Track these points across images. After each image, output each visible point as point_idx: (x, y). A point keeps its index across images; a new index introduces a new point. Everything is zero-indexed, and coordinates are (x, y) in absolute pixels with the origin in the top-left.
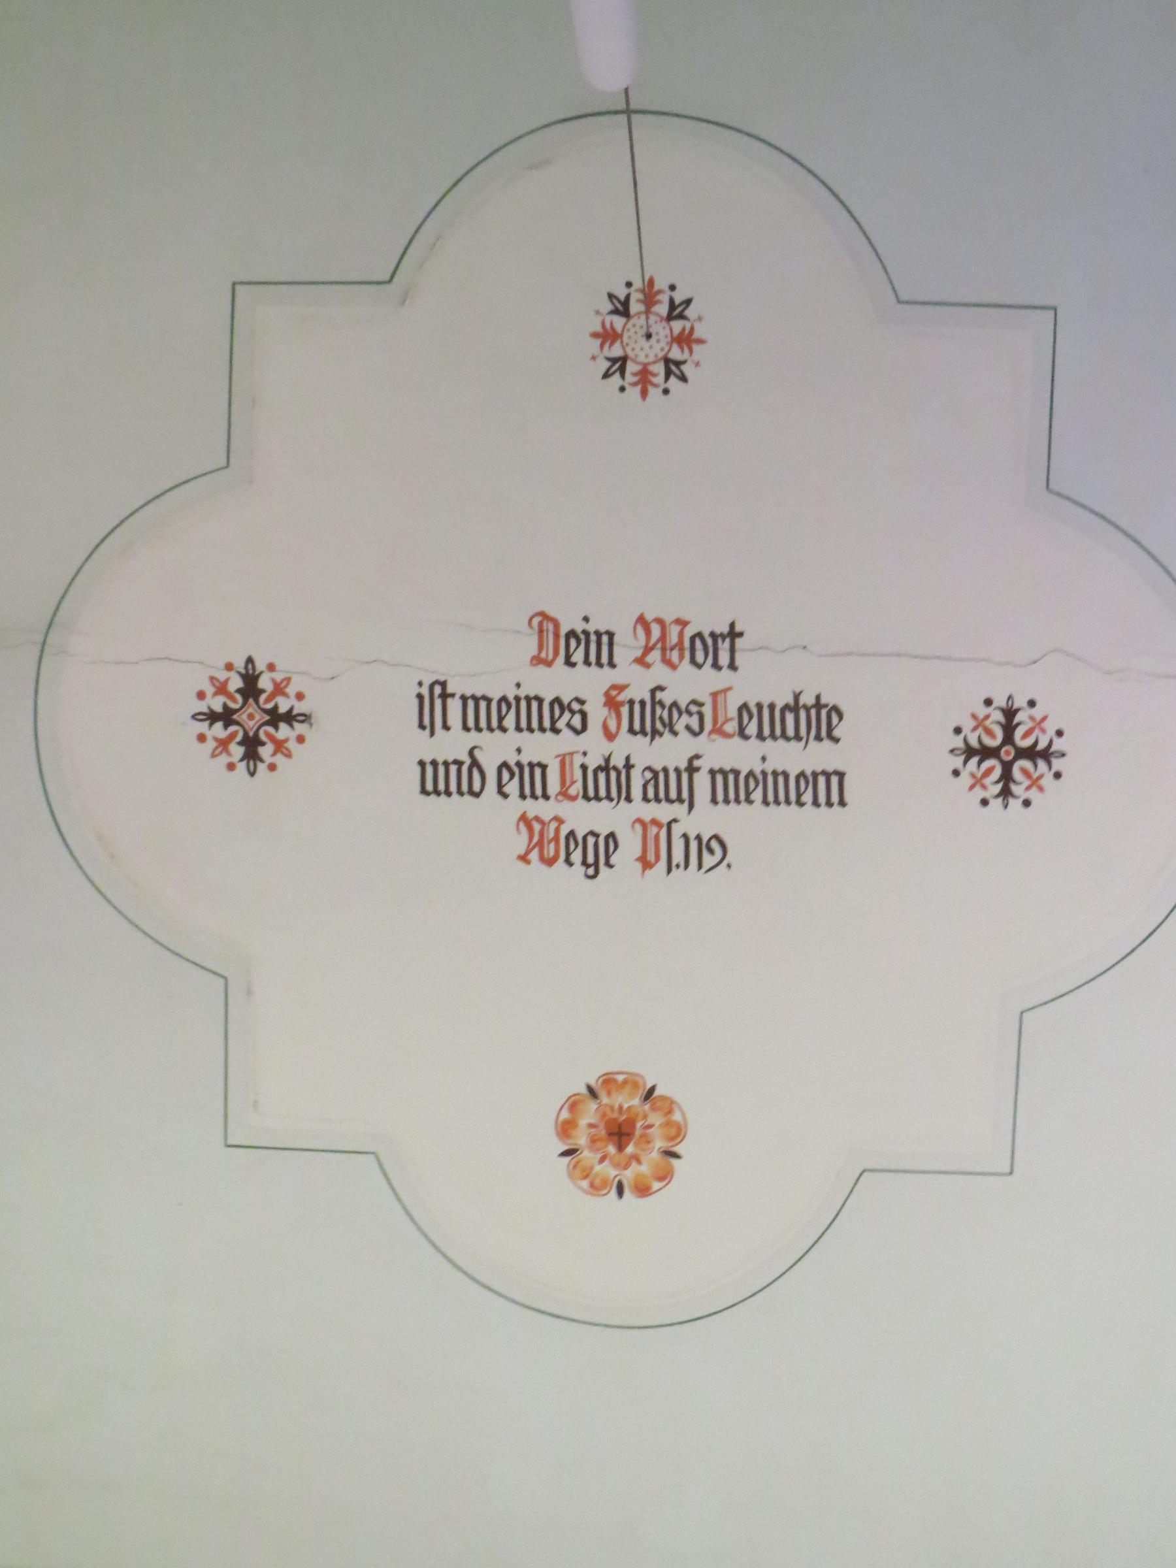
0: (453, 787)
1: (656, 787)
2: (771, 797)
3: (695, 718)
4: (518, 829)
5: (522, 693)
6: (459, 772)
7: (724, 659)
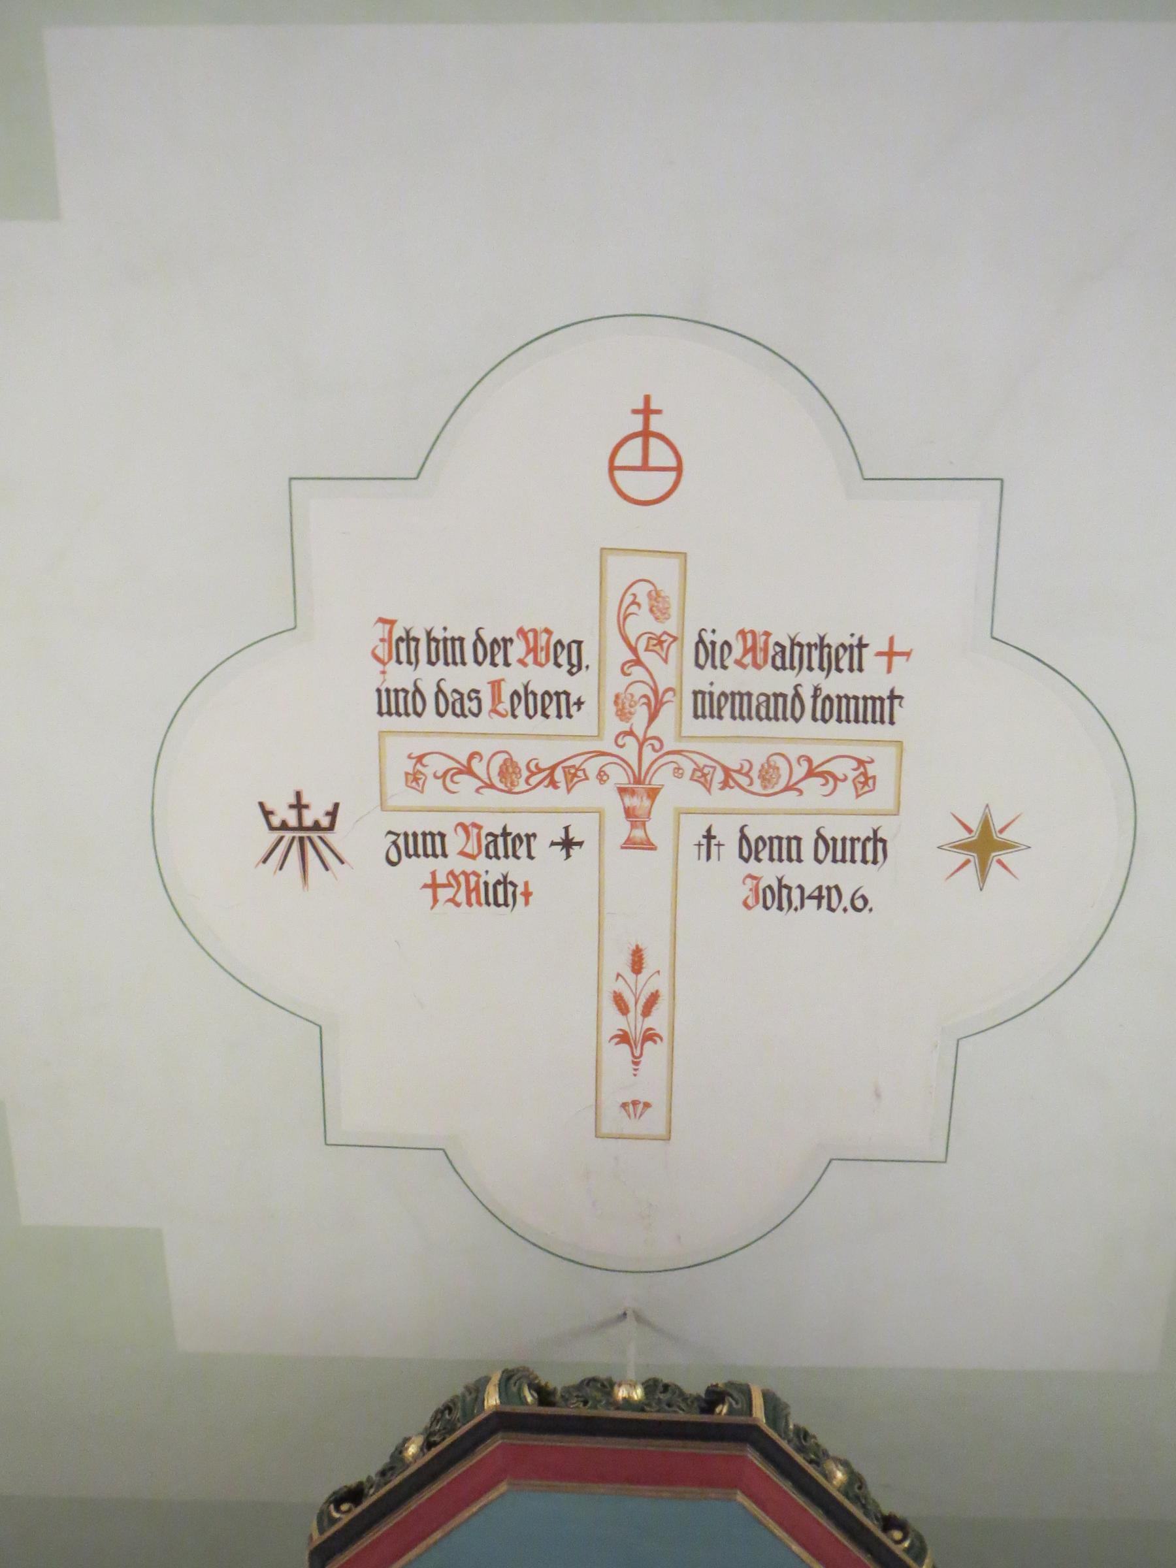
0: (707, 712)
1: (783, 658)
2: (776, 856)
3: (475, 702)
4: (612, 1038)
5: (449, 635)
6: (535, 699)
7: (499, 659)
